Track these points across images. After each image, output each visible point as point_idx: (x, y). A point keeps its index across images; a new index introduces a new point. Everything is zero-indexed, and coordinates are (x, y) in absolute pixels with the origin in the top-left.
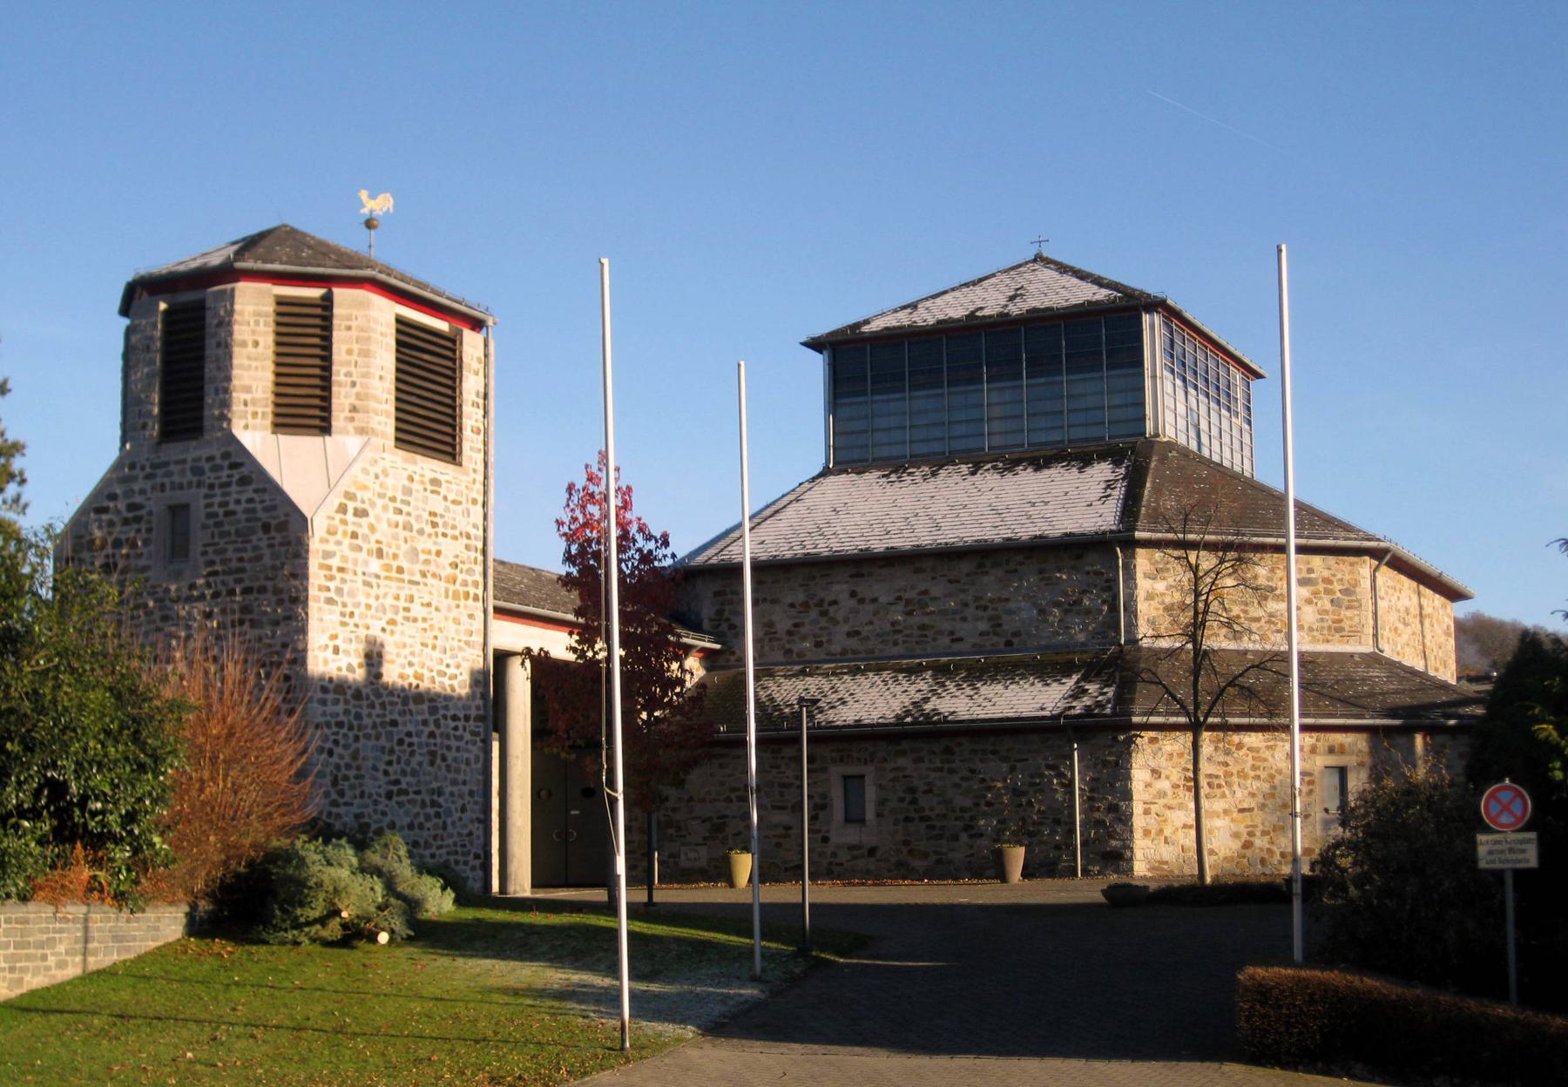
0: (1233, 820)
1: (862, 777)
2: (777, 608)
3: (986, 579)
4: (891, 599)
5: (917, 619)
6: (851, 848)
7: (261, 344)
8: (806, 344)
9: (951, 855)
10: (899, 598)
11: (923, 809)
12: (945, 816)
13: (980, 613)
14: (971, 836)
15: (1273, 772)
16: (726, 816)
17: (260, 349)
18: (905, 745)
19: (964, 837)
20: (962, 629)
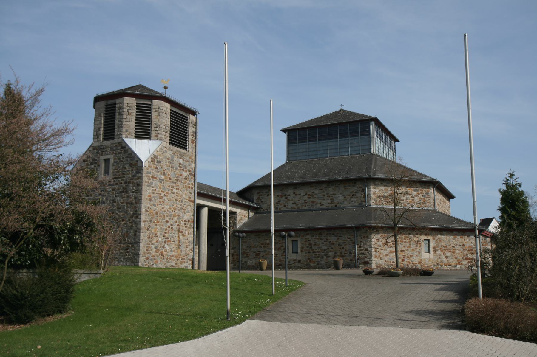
1: (297, 241)
3: (330, 189)
4: (304, 194)
5: (312, 199)
6: (294, 260)
8: (282, 130)
10: (306, 194)
13: (328, 198)
16: (260, 251)
18: (309, 232)
19: (325, 257)
20: (323, 202)
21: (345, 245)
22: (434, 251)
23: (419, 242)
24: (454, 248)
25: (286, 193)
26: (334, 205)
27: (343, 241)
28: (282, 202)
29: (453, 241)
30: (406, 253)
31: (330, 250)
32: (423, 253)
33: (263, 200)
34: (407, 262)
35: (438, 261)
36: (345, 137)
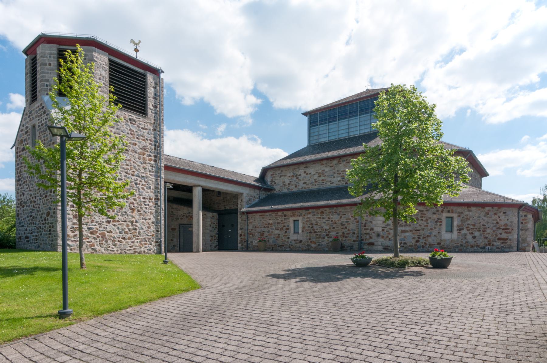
0: (413, 234)
1: (299, 220)
2: (286, 177)
3: (341, 165)
4: (315, 173)
5: (322, 178)
6: (295, 240)
7: (52, 64)
8: (302, 114)
9: (322, 243)
10: (317, 173)
11: (314, 230)
12: (321, 232)
13: (339, 175)
14: (328, 237)
15: (428, 218)
17: (51, 67)
18: (310, 211)
19: (326, 238)
20: (333, 180)
21: (348, 224)
22: (458, 230)
23: (439, 220)
24: (484, 227)
25: (297, 173)
26: (345, 182)
27: (346, 219)
28: (293, 182)
29: (484, 218)
30: (422, 232)
31: (332, 229)
32: (443, 232)
33: (276, 181)
34: (422, 243)
35: (462, 242)
36: (366, 113)
